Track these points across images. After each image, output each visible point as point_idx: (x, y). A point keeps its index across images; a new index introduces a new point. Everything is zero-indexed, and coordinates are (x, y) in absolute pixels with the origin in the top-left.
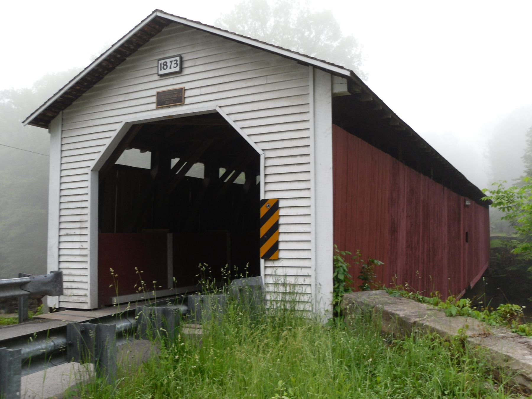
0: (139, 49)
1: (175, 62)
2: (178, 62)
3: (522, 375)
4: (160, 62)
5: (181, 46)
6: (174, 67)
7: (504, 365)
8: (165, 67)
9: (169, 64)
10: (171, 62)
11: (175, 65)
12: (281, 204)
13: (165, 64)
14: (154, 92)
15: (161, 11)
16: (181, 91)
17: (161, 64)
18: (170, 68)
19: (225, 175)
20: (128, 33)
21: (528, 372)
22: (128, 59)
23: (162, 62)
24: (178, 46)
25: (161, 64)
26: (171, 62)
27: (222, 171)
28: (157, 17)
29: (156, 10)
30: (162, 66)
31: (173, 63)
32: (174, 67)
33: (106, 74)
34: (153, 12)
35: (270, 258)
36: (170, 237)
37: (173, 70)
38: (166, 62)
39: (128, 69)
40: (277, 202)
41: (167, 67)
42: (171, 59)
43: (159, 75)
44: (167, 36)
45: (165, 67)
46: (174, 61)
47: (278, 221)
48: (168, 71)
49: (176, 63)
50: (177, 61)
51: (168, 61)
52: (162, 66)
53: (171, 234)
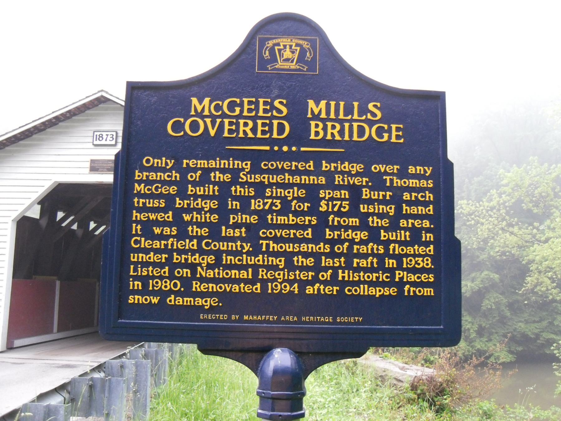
0: (74, 118)
1: (111, 136)
2: (114, 137)
3: (395, 378)
4: (96, 133)
5: (117, 123)
7: (384, 374)
8: (101, 139)
9: (105, 137)
10: (107, 135)
11: (111, 139)
13: (101, 136)
14: (89, 158)
15: (107, 93)
17: (96, 135)
18: (106, 140)
19: (63, 219)
20: (71, 105)
21: (398, 376)
22: (60, 124)
23: (98, 133)
24: (114, 123)
25: (96, 135)
26: (107, 135)
27: (60, 215)
28: (102, 96)
29: (102, 91)
30: (98, 137)
31: (109, 136)
33: (36, 133)
34: (99, 92)
36: (58, 283)
37: (108, 142)
38: (102, 135)
39: (60, 133)
41: (103, 139)
42: (107, 133)
43: (93, 144)
44: (104, 112)
45: (101, 139)
48: (104, 142)
49: (112, 137)
50: (113, 135)
51: (104, 134)
52: (98, 137)
53: (59, 282)
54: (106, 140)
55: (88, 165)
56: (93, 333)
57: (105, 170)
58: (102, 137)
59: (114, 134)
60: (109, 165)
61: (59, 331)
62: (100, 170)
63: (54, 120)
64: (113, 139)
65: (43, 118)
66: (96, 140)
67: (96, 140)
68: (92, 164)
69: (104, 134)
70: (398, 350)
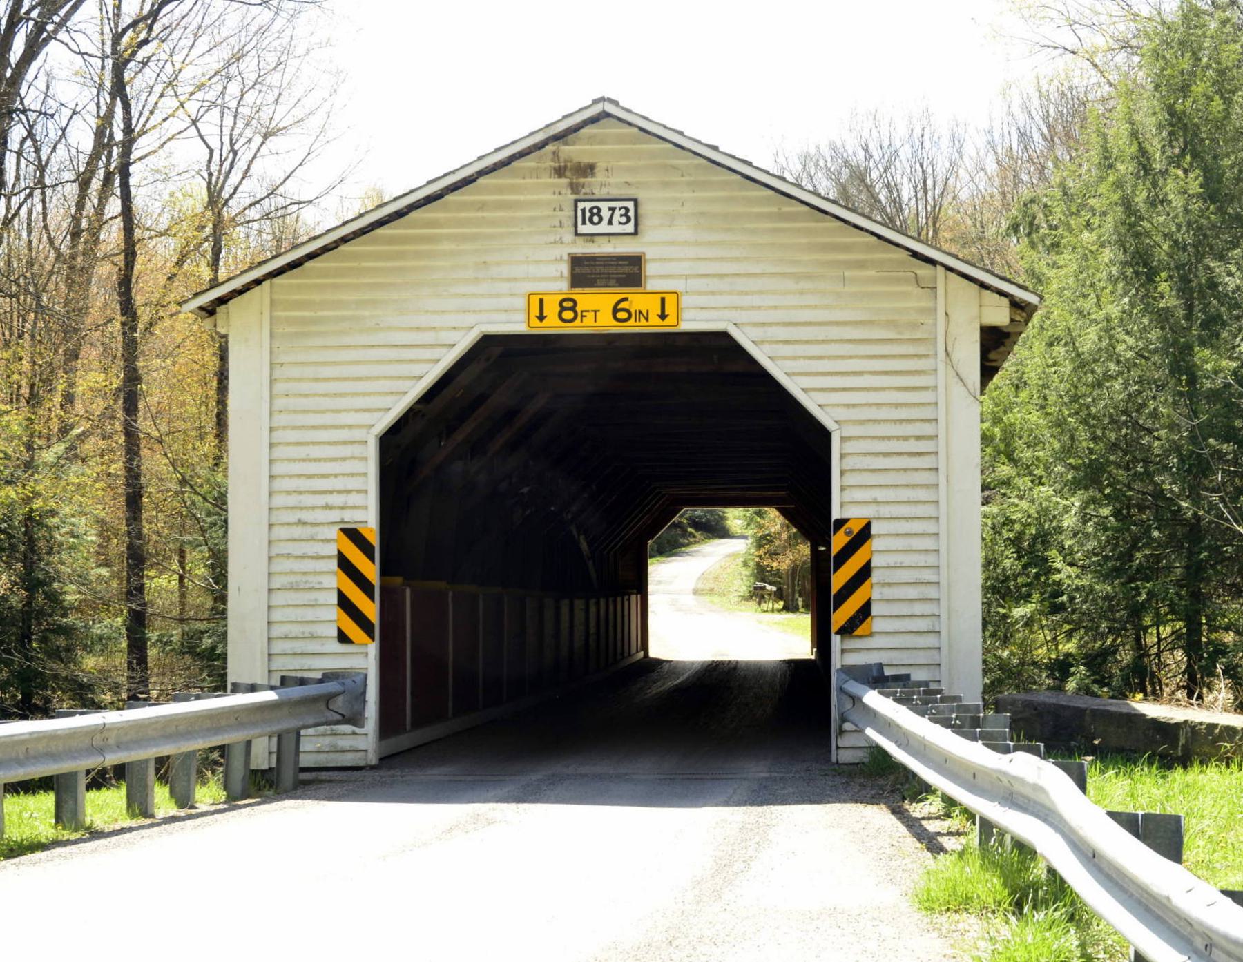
2: (631, 214)
4: (581, 205)
6: (620, 223)
9: (606, 214)
10: (612, 209)
11: (624, 219)
12: (874, 530)
15: (616, 103)
16: (636, 261)
17: (583, 210)
18: (610, 223)
23: (588, 205)
25: (583, 210)
26: (612, 209)
29: (603, 99)
30: (588, 215)
31: (617, 213)
32: (620, 223)
34: (595, 102)
35: (856, 633)
37: (616, 228)
38: (599, 210)
40: (868, 526)
45: (596, 219)
46: (620, 209)
47: (869, 562)
48: (603, 228)
49: (626, 215)
51: (604, 206)
52: (588, 215)
54: (610, 223)
55: (565, 269)
56: (410, 750)
57: (613, 282)
58: (598, 214)
59: (630, 205)
60: (621, 270)
61: (416, 724)
62: (599, 284)
63: (419, 407)
64: (629, 220)
65: (453, 172)
66: (584, 223)
67: (584, 223)
68: (578, 270)
69: (604, 206)
70: (393, 776)
